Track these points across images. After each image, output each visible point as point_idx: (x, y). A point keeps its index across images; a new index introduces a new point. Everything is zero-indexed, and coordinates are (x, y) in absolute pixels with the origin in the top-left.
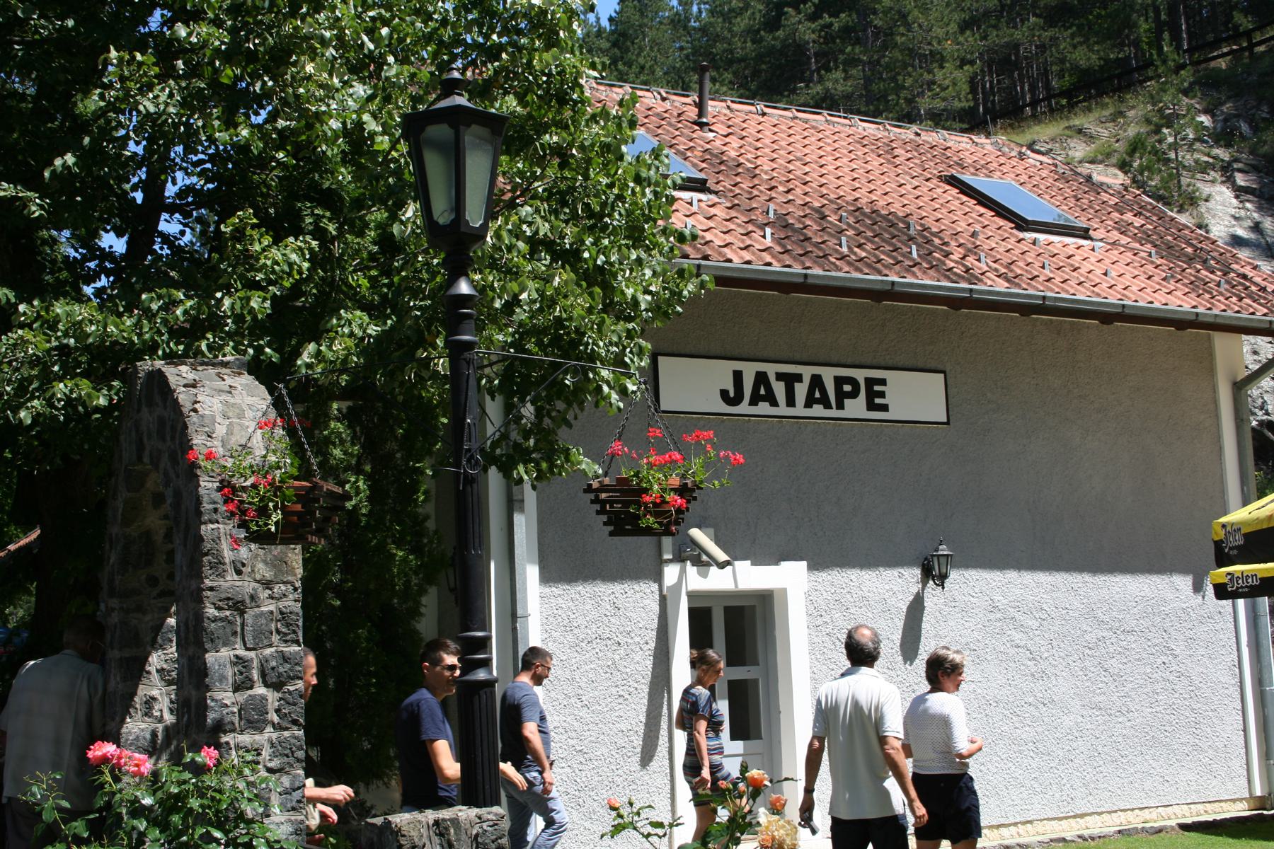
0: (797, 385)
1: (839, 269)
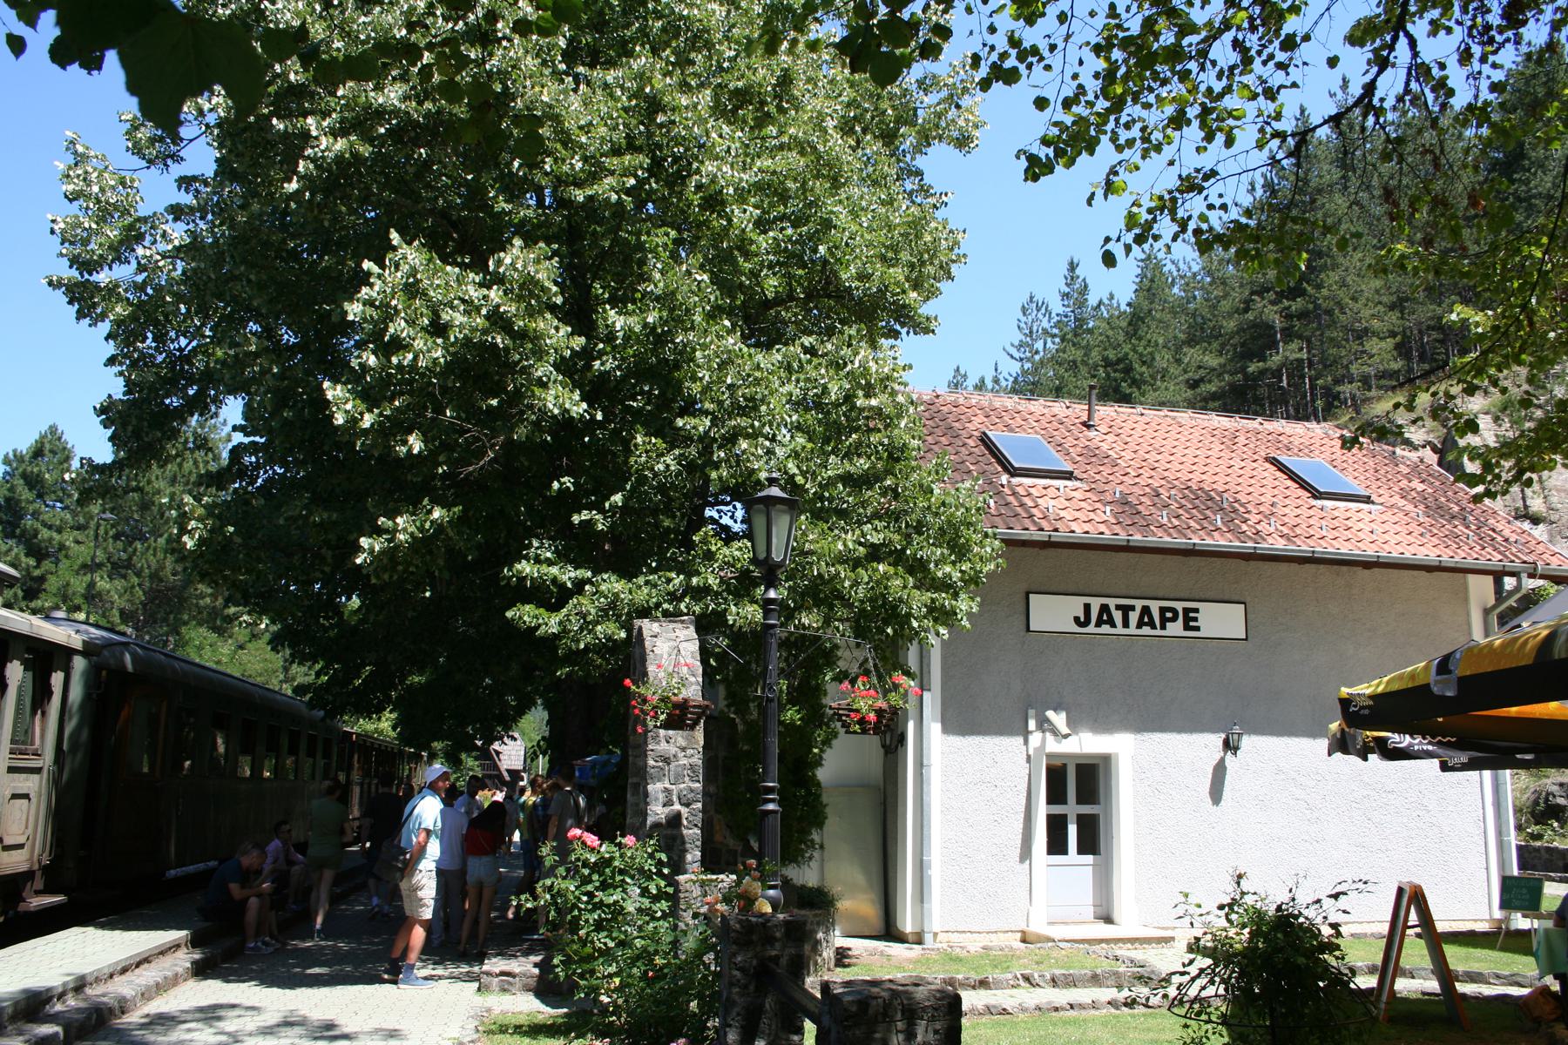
0: (1131, 614)
1: (1154, 535)
